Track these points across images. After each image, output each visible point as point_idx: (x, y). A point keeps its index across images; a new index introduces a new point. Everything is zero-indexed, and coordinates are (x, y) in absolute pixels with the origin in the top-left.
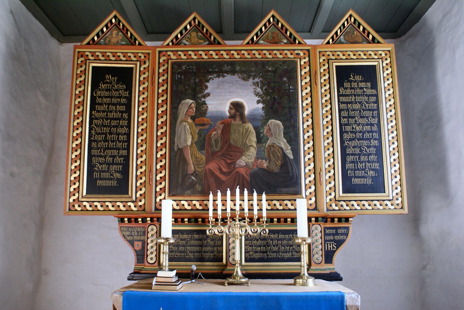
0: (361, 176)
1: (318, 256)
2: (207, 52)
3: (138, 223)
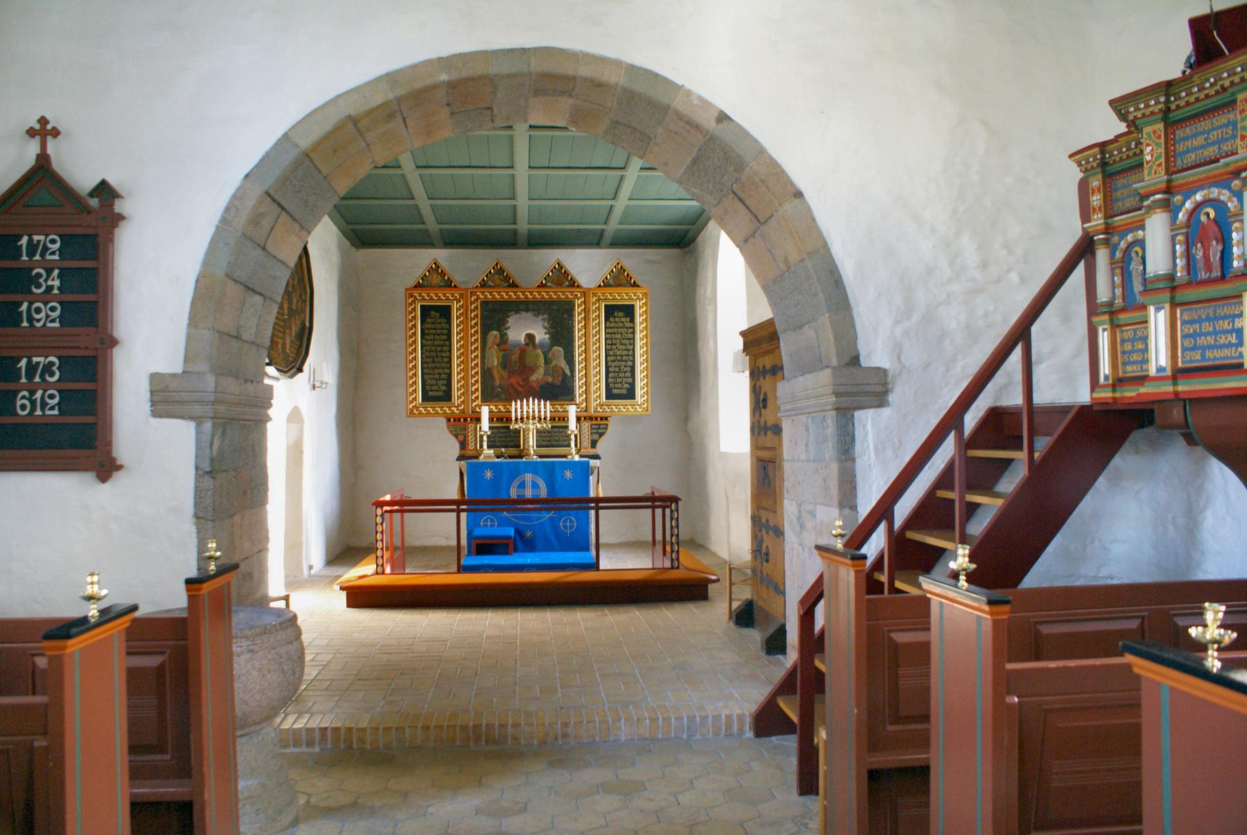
0: (620, 389)
1: (586, 442)
2: (555, 293)
3: (461, 424)
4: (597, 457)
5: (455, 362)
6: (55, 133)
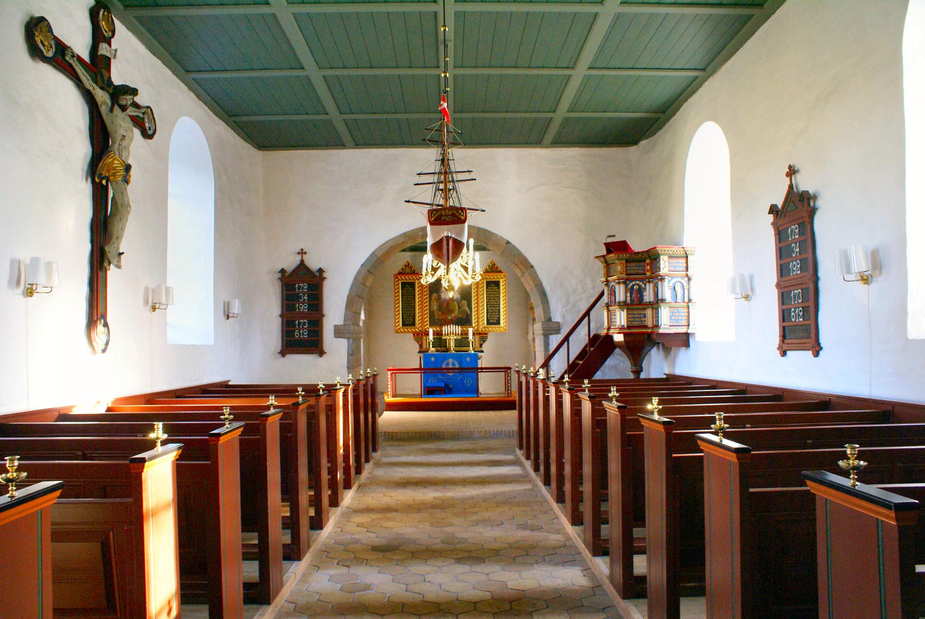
0: (493, 320)
1: (478, 345)
3: (420, 336)
4: (482, 352)
5: (417, 308)
6: (305, 253)
